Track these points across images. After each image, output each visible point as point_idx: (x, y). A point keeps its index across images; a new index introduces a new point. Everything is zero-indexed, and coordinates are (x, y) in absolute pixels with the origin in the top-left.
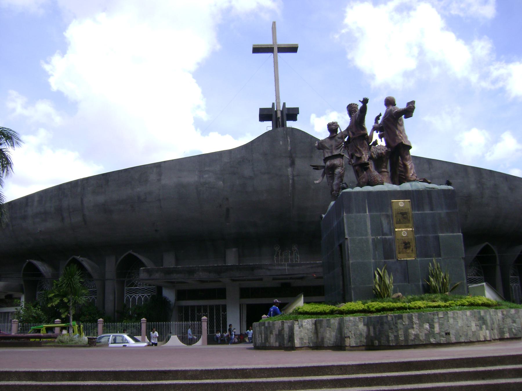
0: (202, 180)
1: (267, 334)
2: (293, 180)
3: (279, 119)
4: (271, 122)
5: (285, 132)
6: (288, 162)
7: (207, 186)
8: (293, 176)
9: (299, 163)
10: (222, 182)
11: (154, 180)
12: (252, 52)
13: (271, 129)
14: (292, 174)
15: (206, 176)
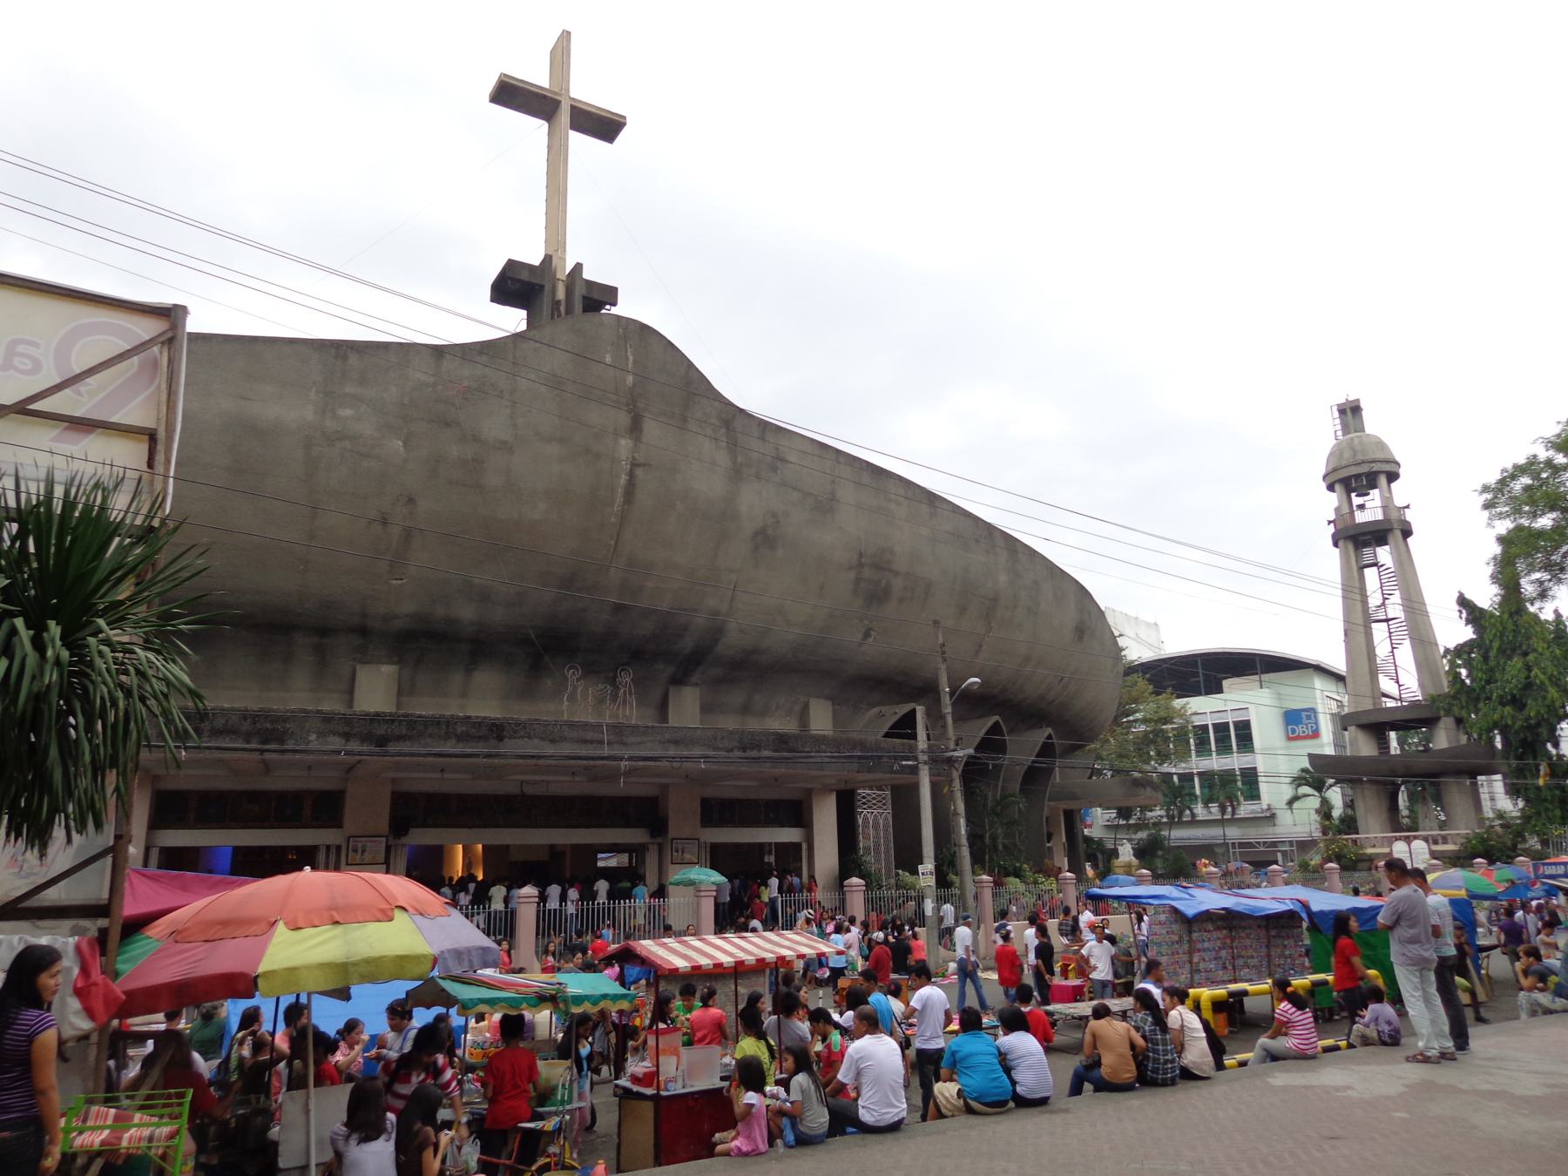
0: (330, 424)
2: (631, 474)
4: (523, 313)
6: (624, 419)
7: (347, 444)
9: (652, 430)
10: (400, 443)
12: (488, 99)
13: (523, 327)
15: (347, 412)
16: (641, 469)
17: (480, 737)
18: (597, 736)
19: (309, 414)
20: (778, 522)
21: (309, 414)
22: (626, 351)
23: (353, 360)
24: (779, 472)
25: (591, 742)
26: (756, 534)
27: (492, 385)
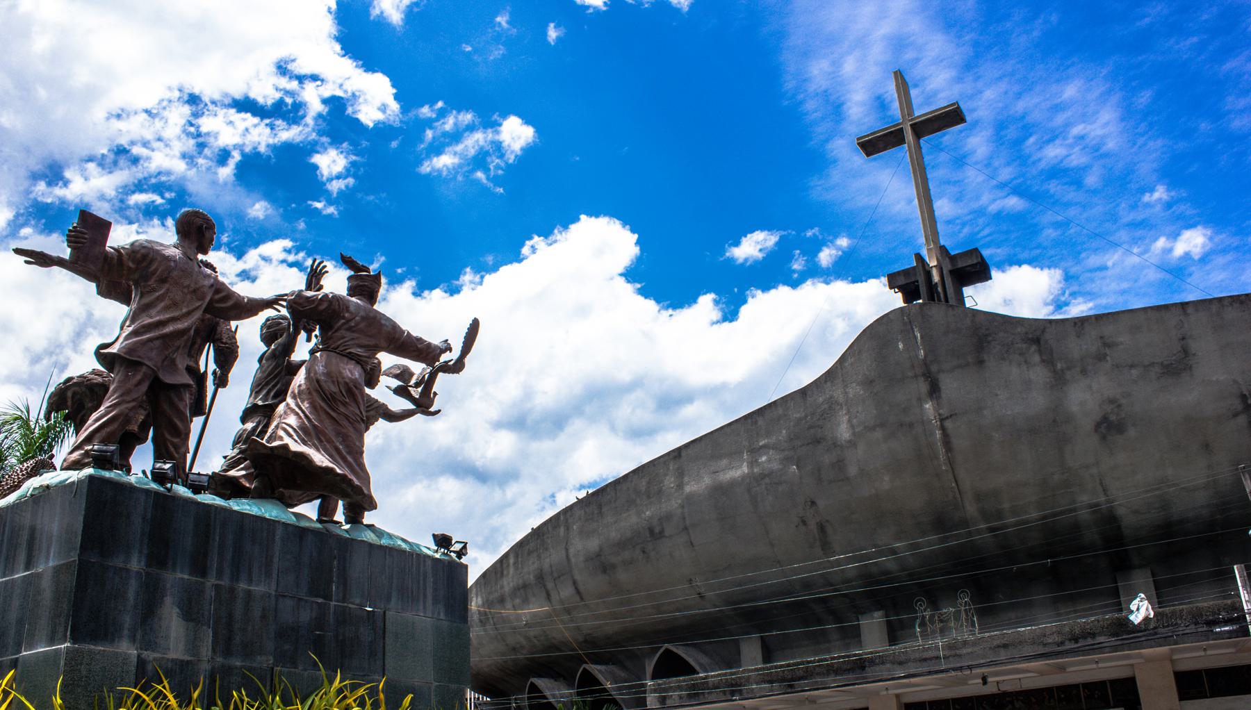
1: (883, 663)
2: (943, 428)
3: (937, 287)
5: (905, 318)
6: (923, 387)
7: (767, 480)
8: (942, 420)
9: (949, 384)
10: (795, 467)
11: (672, 488)
14: (936, 415)
16: (950, 420)
17: (849, 670)
18: (934, 654)
19: (745, 469)
20: (1119, 406)
21: (745, 469)
22: (913, 332)
23: (761, 422)
24: (1108, 358)
25: (931, 659)
26: (1098, 426)
27: (836, 402)
